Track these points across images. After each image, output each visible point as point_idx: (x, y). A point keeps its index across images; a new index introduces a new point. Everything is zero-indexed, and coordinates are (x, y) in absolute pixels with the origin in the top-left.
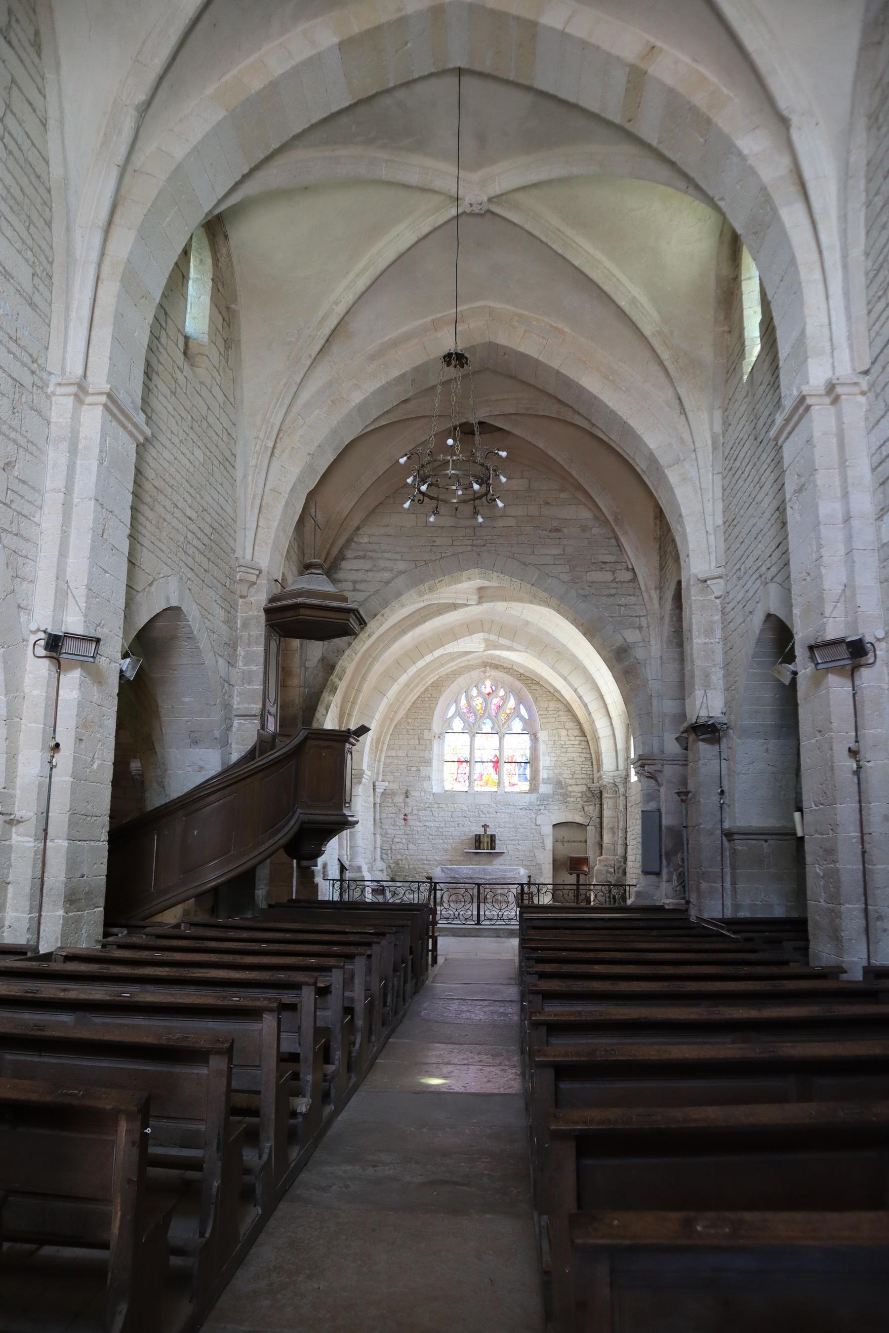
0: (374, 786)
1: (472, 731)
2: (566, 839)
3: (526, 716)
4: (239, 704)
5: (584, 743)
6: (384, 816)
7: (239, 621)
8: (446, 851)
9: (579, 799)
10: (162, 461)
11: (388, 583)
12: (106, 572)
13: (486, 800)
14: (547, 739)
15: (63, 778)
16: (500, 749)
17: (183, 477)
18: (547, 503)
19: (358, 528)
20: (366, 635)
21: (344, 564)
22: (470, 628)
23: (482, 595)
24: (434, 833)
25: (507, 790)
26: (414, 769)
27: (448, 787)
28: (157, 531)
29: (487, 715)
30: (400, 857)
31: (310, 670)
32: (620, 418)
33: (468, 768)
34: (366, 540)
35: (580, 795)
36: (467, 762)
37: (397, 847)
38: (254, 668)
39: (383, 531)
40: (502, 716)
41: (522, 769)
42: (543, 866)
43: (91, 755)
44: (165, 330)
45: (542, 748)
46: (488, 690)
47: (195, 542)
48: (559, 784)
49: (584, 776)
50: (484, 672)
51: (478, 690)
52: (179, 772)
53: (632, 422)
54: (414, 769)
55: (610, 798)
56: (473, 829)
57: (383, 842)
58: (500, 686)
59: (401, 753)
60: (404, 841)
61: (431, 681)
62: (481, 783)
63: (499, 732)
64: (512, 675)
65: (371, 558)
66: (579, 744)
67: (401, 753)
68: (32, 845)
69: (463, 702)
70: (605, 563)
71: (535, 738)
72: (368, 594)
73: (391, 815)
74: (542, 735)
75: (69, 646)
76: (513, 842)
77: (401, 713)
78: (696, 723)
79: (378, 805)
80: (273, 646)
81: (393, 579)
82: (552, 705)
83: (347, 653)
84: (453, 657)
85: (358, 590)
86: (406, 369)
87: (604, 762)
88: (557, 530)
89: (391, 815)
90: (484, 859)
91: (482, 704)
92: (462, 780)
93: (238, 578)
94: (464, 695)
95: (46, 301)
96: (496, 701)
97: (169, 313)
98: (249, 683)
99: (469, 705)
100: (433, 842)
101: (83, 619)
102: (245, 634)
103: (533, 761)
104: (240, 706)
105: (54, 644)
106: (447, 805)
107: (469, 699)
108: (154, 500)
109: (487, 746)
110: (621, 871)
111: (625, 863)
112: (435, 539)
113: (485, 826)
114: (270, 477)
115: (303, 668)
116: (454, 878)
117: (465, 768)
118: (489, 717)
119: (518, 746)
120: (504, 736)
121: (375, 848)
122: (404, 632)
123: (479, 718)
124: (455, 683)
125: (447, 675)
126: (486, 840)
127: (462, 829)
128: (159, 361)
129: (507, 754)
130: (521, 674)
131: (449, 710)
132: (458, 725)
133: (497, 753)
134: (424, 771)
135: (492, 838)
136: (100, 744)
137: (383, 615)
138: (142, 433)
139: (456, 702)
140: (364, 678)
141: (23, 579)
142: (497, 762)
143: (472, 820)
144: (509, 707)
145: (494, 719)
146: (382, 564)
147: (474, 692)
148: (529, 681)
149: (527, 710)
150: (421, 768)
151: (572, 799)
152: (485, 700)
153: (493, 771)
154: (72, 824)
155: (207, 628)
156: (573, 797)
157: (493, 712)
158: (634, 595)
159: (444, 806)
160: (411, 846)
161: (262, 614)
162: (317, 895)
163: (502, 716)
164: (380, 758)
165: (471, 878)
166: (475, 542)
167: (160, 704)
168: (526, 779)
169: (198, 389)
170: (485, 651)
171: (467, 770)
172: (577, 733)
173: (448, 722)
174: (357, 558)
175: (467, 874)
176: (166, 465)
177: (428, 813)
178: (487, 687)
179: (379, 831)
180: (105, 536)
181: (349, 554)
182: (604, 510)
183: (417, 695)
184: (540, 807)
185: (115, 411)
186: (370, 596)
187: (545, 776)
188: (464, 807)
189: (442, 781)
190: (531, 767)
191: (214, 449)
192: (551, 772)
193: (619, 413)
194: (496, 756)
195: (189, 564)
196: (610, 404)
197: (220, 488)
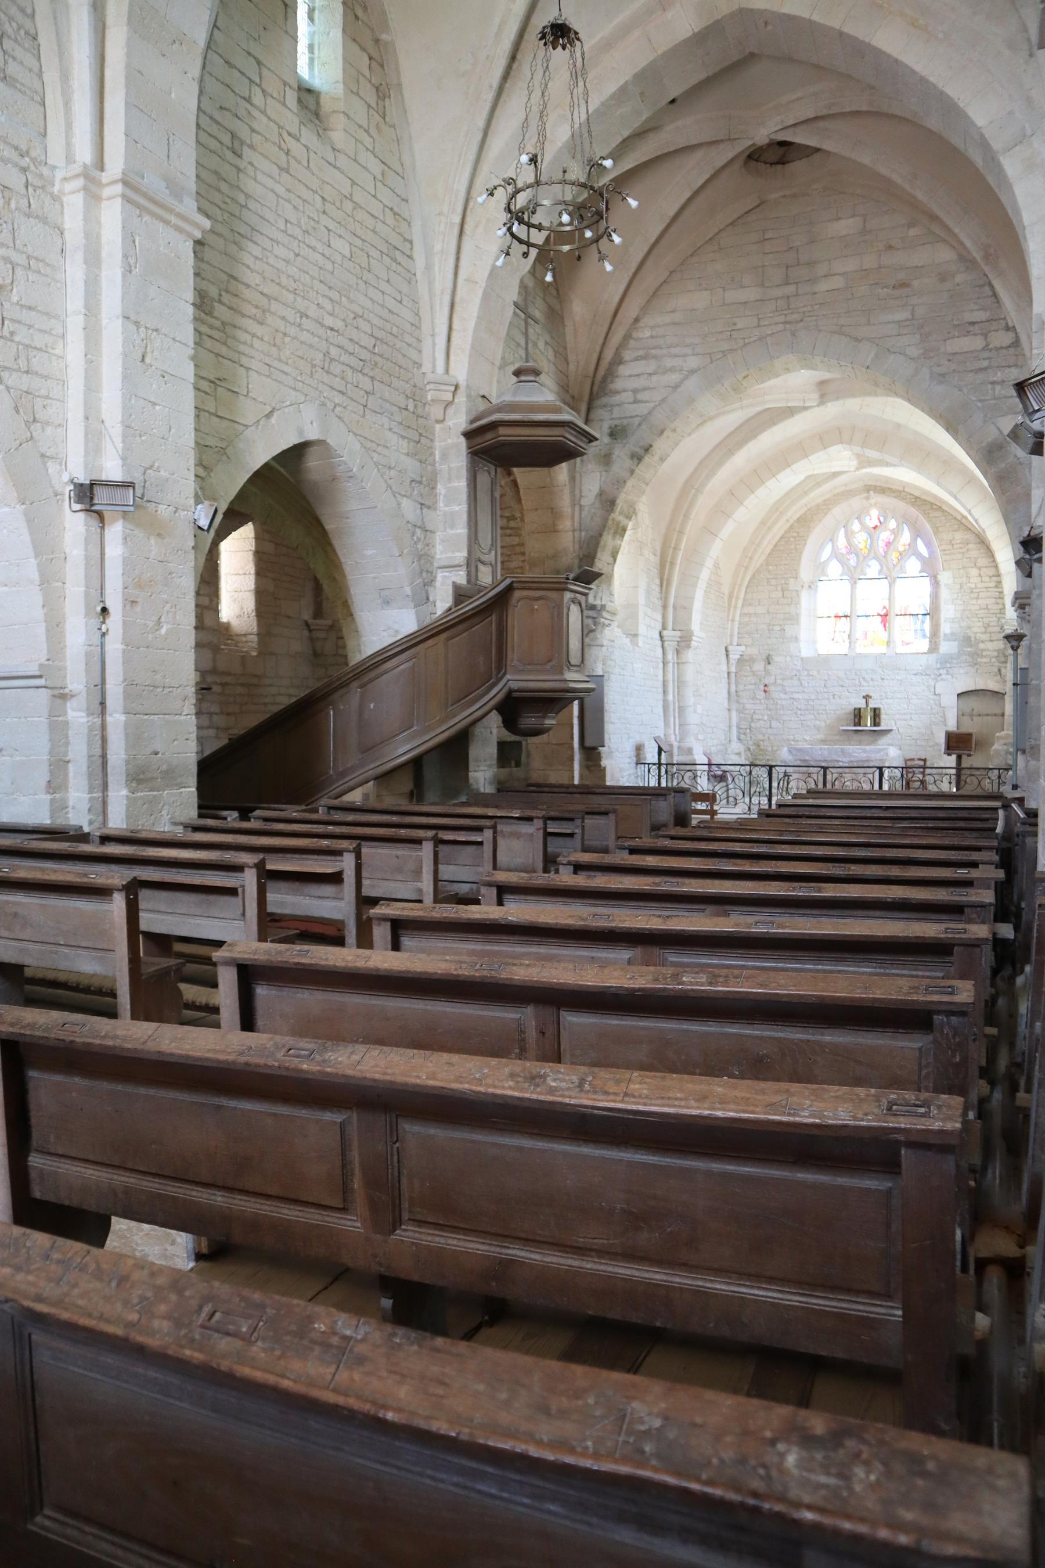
0: (727, 651)
1: (854, 577)
2: (975, 712)
4: (441, 553)
7: (437, 452)
8: (818, 728)
9: (993, 660)
10: (271, 261)
11: (676, 387)
12: (154, 404)
14: (951, 581)
15: (114, 646)
17: (313, 278)
18: (890, 247)
19: (637, 320)
20: (656, 458)
21: (623, 370)
22: (824, 439)
23: (825, 392)
26: (778, 628)
28: (274, 350)
29: (872, 554)
30: (761, 737)
31: (586, 509)
32: (935, 86)
34: (648, 334)
35: (996, 654)
36: (846, 616)
37: (758, 725)
38: (457, 509)
39: (668, 319)
40: (894, 556)
41: (919, 623)
43: (155, 618)
44: (260, 86)
45: (944, 594)
47: (345, 358)
48: (967, 640)
50: (867, 498)
51: (861, 524)
52: (375, 638)
53: (949, 91)
56: (853, 701)
59: (760, 610)
60: (766, 718)
61: (797, 516)
63: (889, 576)
64: (903, 499)
65: (655, 357)
67: (760, 610)
68: (85, 720)
69: (842, 541)
70: (973, 323)
71: (935, 583)
72: (652, 405)
73: (750, 687)
74: (945, 578)
75: (101, 496)
76: (904, 717)
77: (759, 560)
78: (1029, 535)
79: (733, 675)
80: (484, 479)
81: (682, 381)
82: (959, 536)
83: (630, 483)
84: (815, 481)
85: (640, 402)
86: (625, 76)
88: (903, 285)
89: (750, 687)
90: (865, 738)
93: (429, 398)
94: (843, 530)
95: (31, 70)
96: (885, 536)
97: (264, 61)
98: (452, 527)
99: (850, 545)
101: (120, 462)
102: (445, 467)
103: (933, 613)
104: (443, 556)
105: (86, 494)
107: (849, 535)
108: (264, 311)
109: (872, 595)
112: (735, 320)
113: (867, 697)
114: (463, 263)
115: (577, 508)
116: (805, 761)
120: (894, 581)
121: (730, 727)
122: (731, 453)
123: (863, 560)
125: (818, 505)
128: (253, 130)
130: (916, 498)
131: (822, 551)
134: (789, 630)
135: (876, 713)
136: (168, 606)
137: (674, 430)
138: (196, 225)
140: (686, 516)
141: (47, 423)
142: (886, 615)
143: (851, 689)
145: (883, 560)
146: (669, 363)
148: (928, 506)
150: (786, 627)
151: (985, 660)
154: (127, 695)
155: (376, 464)
157: (881, 550)
158: (1016, 366)
159: (815, 673)
160: (774, 724)
161: (463, 440)
162: (605, 781)
163: (894, 556)
164: (734, 616)
166: (790, 318)
167: (343, 560)
168: (924, 636)
169: (331, 160)
170: (857, 469)
173: (821, 568)
174: (637, 359)
176: (281, 265)
177: (796, 682)
178: (873, 518)
179: (734, 706)
180: (148, 360)
181: (627, 355)
182: (968, 243)
183: (781, 533)
184: (941, 671)
185: (142, 201)
186: (654, 408)
189: (815, 642)
190: (932, 619)
191: (369, 236)
193: (932, 79)
195: (336, 386)
196: (918, 68)
197: (384, 286)
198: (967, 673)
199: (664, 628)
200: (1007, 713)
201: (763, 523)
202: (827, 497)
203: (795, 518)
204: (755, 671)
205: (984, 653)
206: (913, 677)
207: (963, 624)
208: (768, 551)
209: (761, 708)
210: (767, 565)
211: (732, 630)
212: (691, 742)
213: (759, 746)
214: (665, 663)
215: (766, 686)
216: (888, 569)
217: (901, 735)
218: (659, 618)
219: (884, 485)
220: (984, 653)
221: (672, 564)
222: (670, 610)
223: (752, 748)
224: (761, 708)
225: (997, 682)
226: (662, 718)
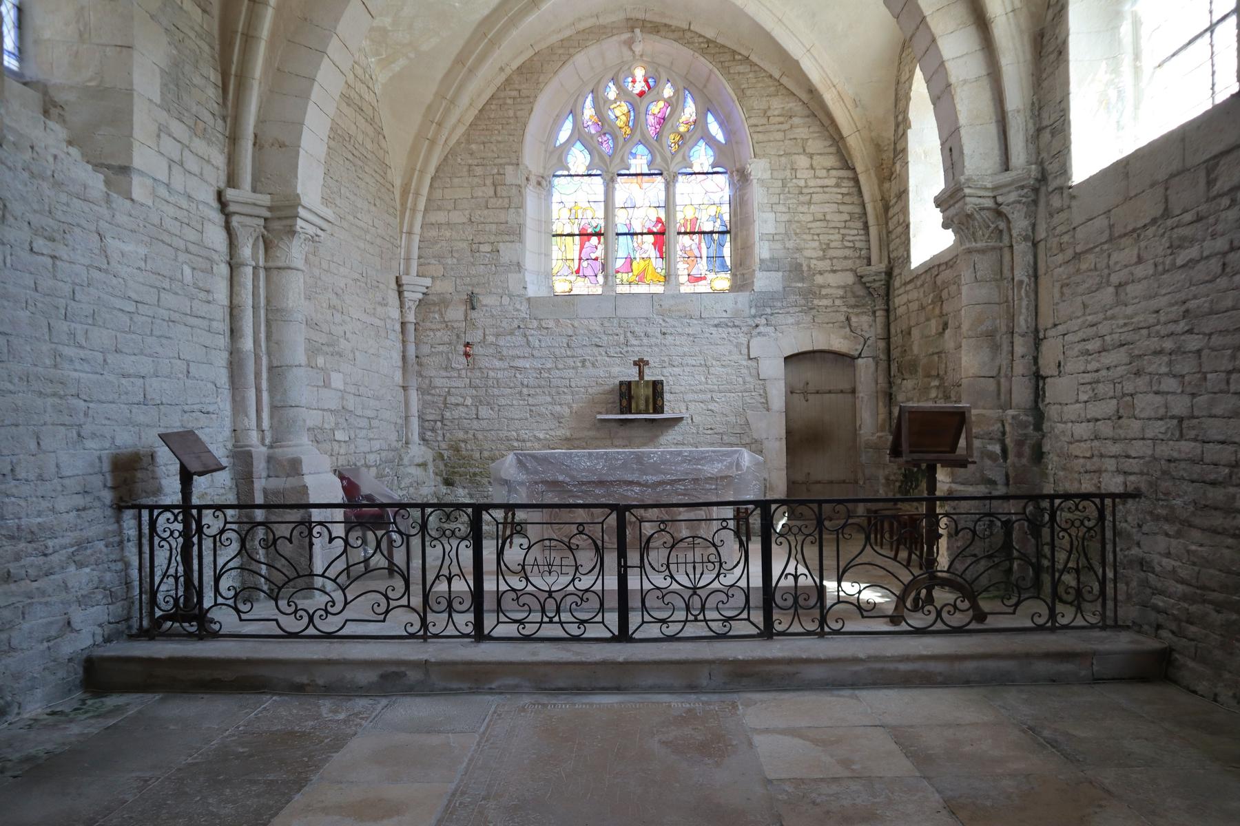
1: (609, 170)
2: (811, 388)
3: (720, 137)
5: (846, 183)
6: (426, 349)
8: (559, 418)
9: (838, 302)
13: (642, 310)
14: (767, 175)
16: (669, 204)
24: (532, 382)
25: (683, 289)
26: (486, 248)
27: (560, 287)
29: (638, 136)
30: (461, 435)
33: (601, 247)
35: (841, 292)
36: (598, 234)
37: (456, 414)
41: (714, 246)
42: (766, 443)
45: (758, 194)
46: (640, 86)
48: (796, 270)
49: (848, 252)
54: (486, 248)
55: (982, 251)
56: (615, 370)
57: (425, 405)
58: (664, 77)
59: (457, 217)
60: (469, 401)
62: (631, 277)
63: (667, 171)
64: (688, 43)
66: (837, 186)
67: (457, 217)
69: (589, 112)
71: (740, 179)
73: (441, 348)
74: (758, 169)
76: (702, 397)
79: (411, 328)
87: (966, 151)
89: (441, 348)
91: (627, 114)
92: (589, 272)
99: (601, 117)
100: (531, 401)
103: (737, 228)
106: (557, 321)
107: (601, 106)
109: (640, 201)
110: (1027, 450)
111: (1038, 427)
113: (640, 364)
116: (554, 485)
117: (595, 247)
118: (644, 141)
119: (704, 197)
121: (407, 418)
124: (568, 68)
125: (551, 48)
126: (644, 392)
127: (592, 371)
129: (683, 215)
130: (709, 41)
131: (560, 125)
132: (578, 159)
133: (662, 214)
134: (507, 253)
135: (657, 387)
139: (575, 112)
142: (662, 233)
143: (612, 351)
144: (683, 119)
145: (654, 145)
147: (612, 93)
148: (728, 57)
149: (721, 125)
150: (501, 247)
151: (825, 302)
152: (633, 107)
153: (653, 253)
156: (826, 296)
157: (652, 131)
159: (551, 324)
160: (484, 412)
164: (411, 225)
165: (601, 483)
168: (723, 267)
171: (599, 253)
172: (831, 161)
173: (558, 157)
175: (588, 470)
177: (519, 340)
178: (638, 79)
179: (414, 382)
184: (757, 321)
187: (766, 255)
188: (595, 326)
190: (734, 241)
192: (778, 246)
194: (659, 220)
198: (798, 323)
199: (232, 181)
200: (860, 388)
201: (460, 60)
202: (567, 33)
203: (515, 65)
204: (451, 317)
205: (824, 292)
206: (713, 330)
207: (790, 244)
208: (470, 118)
209: (459, 383)
210: (468, 142)
211: (408, 251)
212: (302, 447)
213: (458, 450)
214: (234, 266)
215: (467, 345)
216: (664, 159)
217: (698, 426)
218: (220, 160)
219: (657, 19)
220: (824, 292)
221: (249, 39)
222: (247, 146)
223: (446, 455)
224: (459, 383)
225: (845, 338)
226: (226, 393)
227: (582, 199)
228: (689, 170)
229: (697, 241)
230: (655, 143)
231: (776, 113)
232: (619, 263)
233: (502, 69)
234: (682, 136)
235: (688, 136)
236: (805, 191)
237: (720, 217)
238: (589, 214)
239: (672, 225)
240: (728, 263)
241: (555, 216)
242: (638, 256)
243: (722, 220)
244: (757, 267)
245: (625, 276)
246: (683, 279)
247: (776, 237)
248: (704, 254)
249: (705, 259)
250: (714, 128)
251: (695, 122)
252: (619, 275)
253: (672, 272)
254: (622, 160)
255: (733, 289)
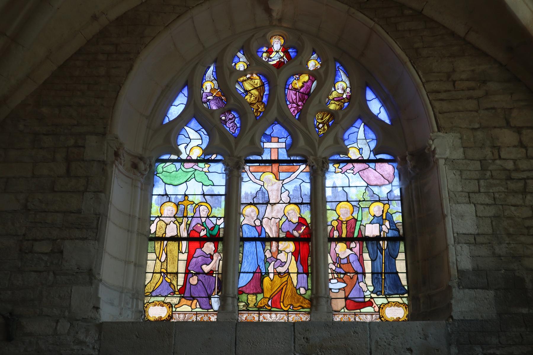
1: (234, 154)
3: (384, 116)
14: (458, 154)
26: (45, 247)
27: (156, 312)
29: (274, 113)
41: (382, 257)
45: (448, 180)
63: (316, 155)
74: (445, 146)
91: (260, 89)
103: (419, 224)
107: (226, 78)
109: (275, 193)
113: (464, 317)
118: (283, 120)
129: (336, 214)
132: (193, 141)
138: (133, 302)
139: (193, 86)
149: (385, 103)
157: (292, 109)
168: (396, 288)
171: (216, 264)
192: (484, 251)
203: (113, 15)
216: (309, 141)
227: (194, 188)
228: (342, 157)
229: (357, 250)
230: (298, 123)
231: (464, 76)
232: (244, 280)
233: (95, 18)
234: (333, 114)
235: (341, 114)
236: (515, 175)
237: (389, 217)
238: (203, 211)
239: (321, 227)
240: (404, 282)
241: (155, 210)
242: (271, 269)
243: (392, 222)
244: (455, 282)
245: (252, 299)
246: (339, 304)
247: (479, 239)
248: (368, 268)
249: (369, 276)
250: (375, 106)
251: (349, 98)
252: (244, 297)
253: (322, 292)
254: (252, 142)
255: (412, 316)
